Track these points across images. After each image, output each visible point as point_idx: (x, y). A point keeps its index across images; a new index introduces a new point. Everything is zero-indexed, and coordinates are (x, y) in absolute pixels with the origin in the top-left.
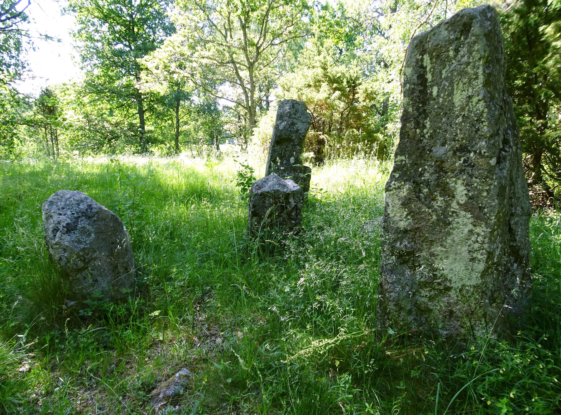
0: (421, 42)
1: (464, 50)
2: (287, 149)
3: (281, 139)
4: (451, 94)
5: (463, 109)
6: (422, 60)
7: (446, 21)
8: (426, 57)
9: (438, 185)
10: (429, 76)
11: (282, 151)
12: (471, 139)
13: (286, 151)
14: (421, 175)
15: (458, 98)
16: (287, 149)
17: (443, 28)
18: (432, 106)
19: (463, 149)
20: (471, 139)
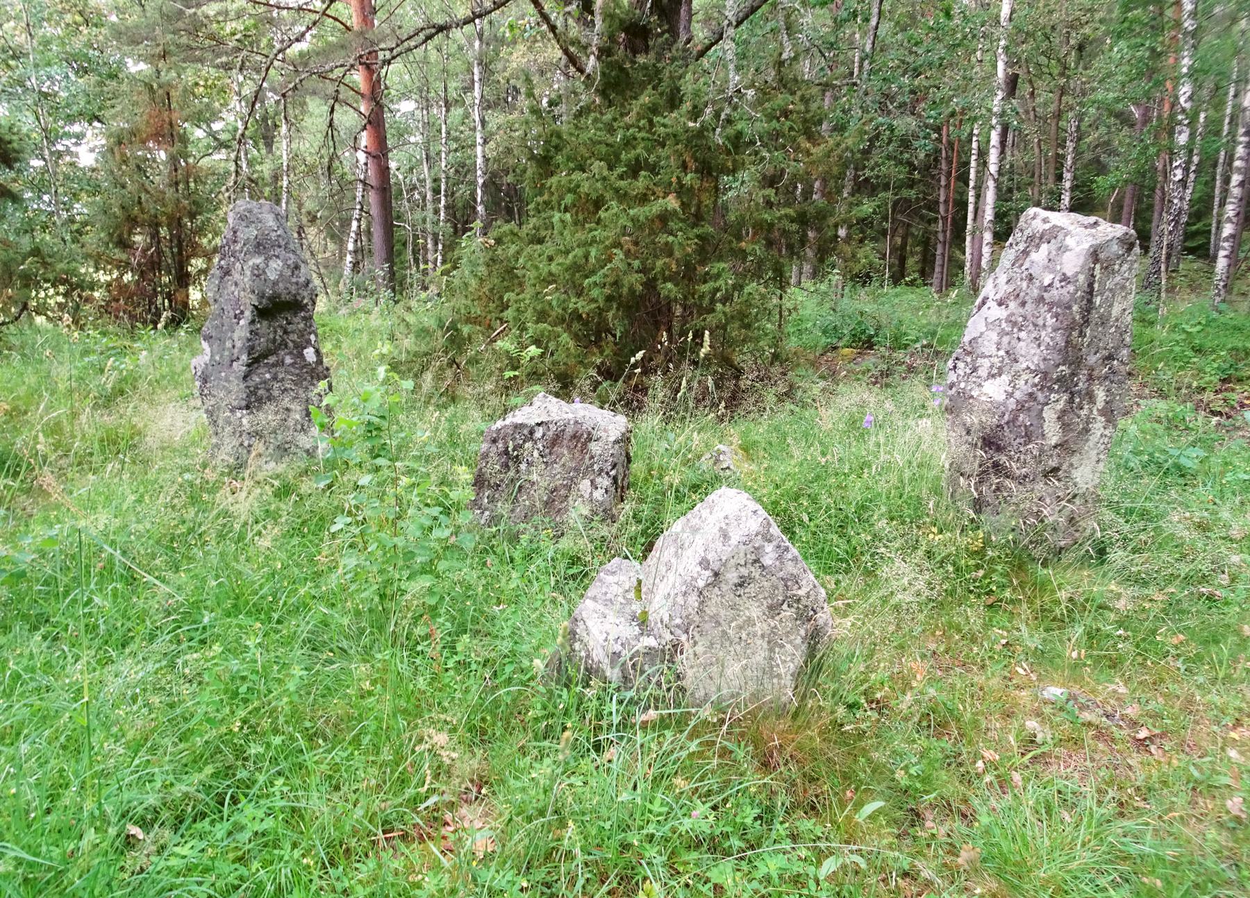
0: (1095, 251)
1: (1125, 267)
2: (290, 328)
3: (275, 304)
4: (1111, 306)
5: (1117, 320)
6: (1094, 269)
7: (384, 101)
8: (1098, 266)
9: (1087, 394)
10: (1096, 286)
11: (275, 332)
12: (1117, 348)
13: (286, 332)
14: (1076, 385)
15: (1116, 310)
16: (290, 328)
17: (1115, 241)
18: (1094, 316)
19: (1110, 357)
20: (1117, 348)
